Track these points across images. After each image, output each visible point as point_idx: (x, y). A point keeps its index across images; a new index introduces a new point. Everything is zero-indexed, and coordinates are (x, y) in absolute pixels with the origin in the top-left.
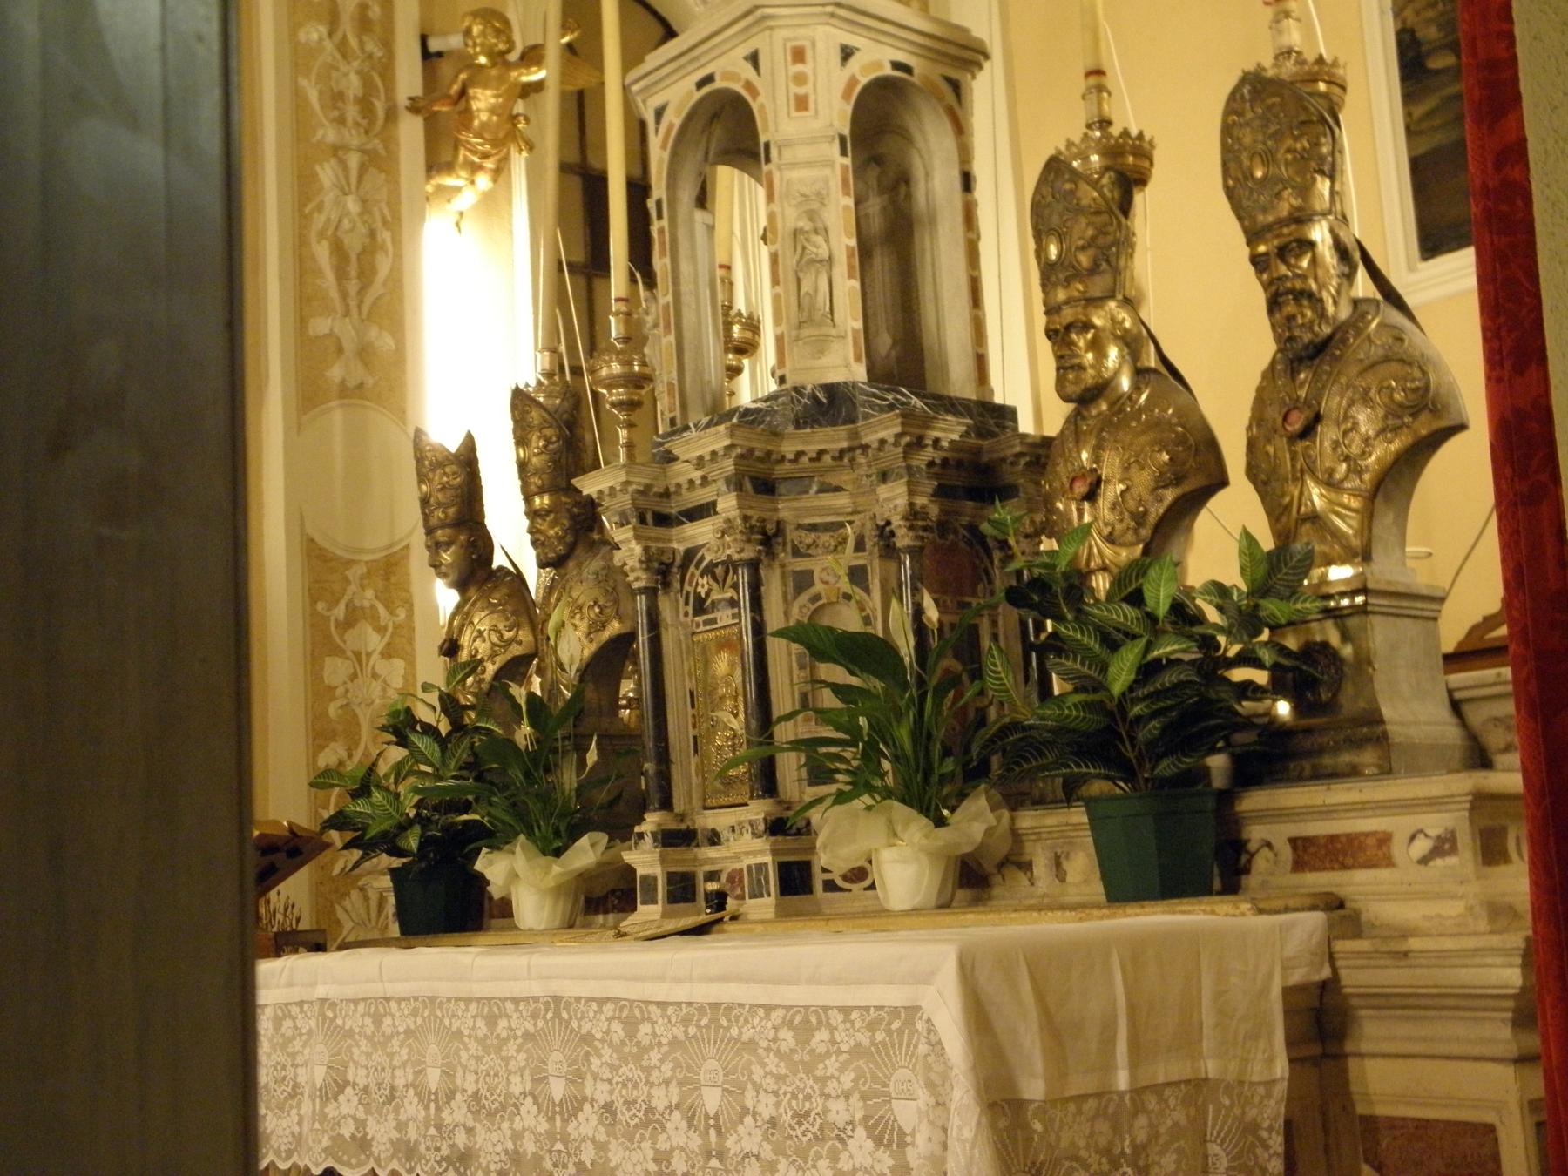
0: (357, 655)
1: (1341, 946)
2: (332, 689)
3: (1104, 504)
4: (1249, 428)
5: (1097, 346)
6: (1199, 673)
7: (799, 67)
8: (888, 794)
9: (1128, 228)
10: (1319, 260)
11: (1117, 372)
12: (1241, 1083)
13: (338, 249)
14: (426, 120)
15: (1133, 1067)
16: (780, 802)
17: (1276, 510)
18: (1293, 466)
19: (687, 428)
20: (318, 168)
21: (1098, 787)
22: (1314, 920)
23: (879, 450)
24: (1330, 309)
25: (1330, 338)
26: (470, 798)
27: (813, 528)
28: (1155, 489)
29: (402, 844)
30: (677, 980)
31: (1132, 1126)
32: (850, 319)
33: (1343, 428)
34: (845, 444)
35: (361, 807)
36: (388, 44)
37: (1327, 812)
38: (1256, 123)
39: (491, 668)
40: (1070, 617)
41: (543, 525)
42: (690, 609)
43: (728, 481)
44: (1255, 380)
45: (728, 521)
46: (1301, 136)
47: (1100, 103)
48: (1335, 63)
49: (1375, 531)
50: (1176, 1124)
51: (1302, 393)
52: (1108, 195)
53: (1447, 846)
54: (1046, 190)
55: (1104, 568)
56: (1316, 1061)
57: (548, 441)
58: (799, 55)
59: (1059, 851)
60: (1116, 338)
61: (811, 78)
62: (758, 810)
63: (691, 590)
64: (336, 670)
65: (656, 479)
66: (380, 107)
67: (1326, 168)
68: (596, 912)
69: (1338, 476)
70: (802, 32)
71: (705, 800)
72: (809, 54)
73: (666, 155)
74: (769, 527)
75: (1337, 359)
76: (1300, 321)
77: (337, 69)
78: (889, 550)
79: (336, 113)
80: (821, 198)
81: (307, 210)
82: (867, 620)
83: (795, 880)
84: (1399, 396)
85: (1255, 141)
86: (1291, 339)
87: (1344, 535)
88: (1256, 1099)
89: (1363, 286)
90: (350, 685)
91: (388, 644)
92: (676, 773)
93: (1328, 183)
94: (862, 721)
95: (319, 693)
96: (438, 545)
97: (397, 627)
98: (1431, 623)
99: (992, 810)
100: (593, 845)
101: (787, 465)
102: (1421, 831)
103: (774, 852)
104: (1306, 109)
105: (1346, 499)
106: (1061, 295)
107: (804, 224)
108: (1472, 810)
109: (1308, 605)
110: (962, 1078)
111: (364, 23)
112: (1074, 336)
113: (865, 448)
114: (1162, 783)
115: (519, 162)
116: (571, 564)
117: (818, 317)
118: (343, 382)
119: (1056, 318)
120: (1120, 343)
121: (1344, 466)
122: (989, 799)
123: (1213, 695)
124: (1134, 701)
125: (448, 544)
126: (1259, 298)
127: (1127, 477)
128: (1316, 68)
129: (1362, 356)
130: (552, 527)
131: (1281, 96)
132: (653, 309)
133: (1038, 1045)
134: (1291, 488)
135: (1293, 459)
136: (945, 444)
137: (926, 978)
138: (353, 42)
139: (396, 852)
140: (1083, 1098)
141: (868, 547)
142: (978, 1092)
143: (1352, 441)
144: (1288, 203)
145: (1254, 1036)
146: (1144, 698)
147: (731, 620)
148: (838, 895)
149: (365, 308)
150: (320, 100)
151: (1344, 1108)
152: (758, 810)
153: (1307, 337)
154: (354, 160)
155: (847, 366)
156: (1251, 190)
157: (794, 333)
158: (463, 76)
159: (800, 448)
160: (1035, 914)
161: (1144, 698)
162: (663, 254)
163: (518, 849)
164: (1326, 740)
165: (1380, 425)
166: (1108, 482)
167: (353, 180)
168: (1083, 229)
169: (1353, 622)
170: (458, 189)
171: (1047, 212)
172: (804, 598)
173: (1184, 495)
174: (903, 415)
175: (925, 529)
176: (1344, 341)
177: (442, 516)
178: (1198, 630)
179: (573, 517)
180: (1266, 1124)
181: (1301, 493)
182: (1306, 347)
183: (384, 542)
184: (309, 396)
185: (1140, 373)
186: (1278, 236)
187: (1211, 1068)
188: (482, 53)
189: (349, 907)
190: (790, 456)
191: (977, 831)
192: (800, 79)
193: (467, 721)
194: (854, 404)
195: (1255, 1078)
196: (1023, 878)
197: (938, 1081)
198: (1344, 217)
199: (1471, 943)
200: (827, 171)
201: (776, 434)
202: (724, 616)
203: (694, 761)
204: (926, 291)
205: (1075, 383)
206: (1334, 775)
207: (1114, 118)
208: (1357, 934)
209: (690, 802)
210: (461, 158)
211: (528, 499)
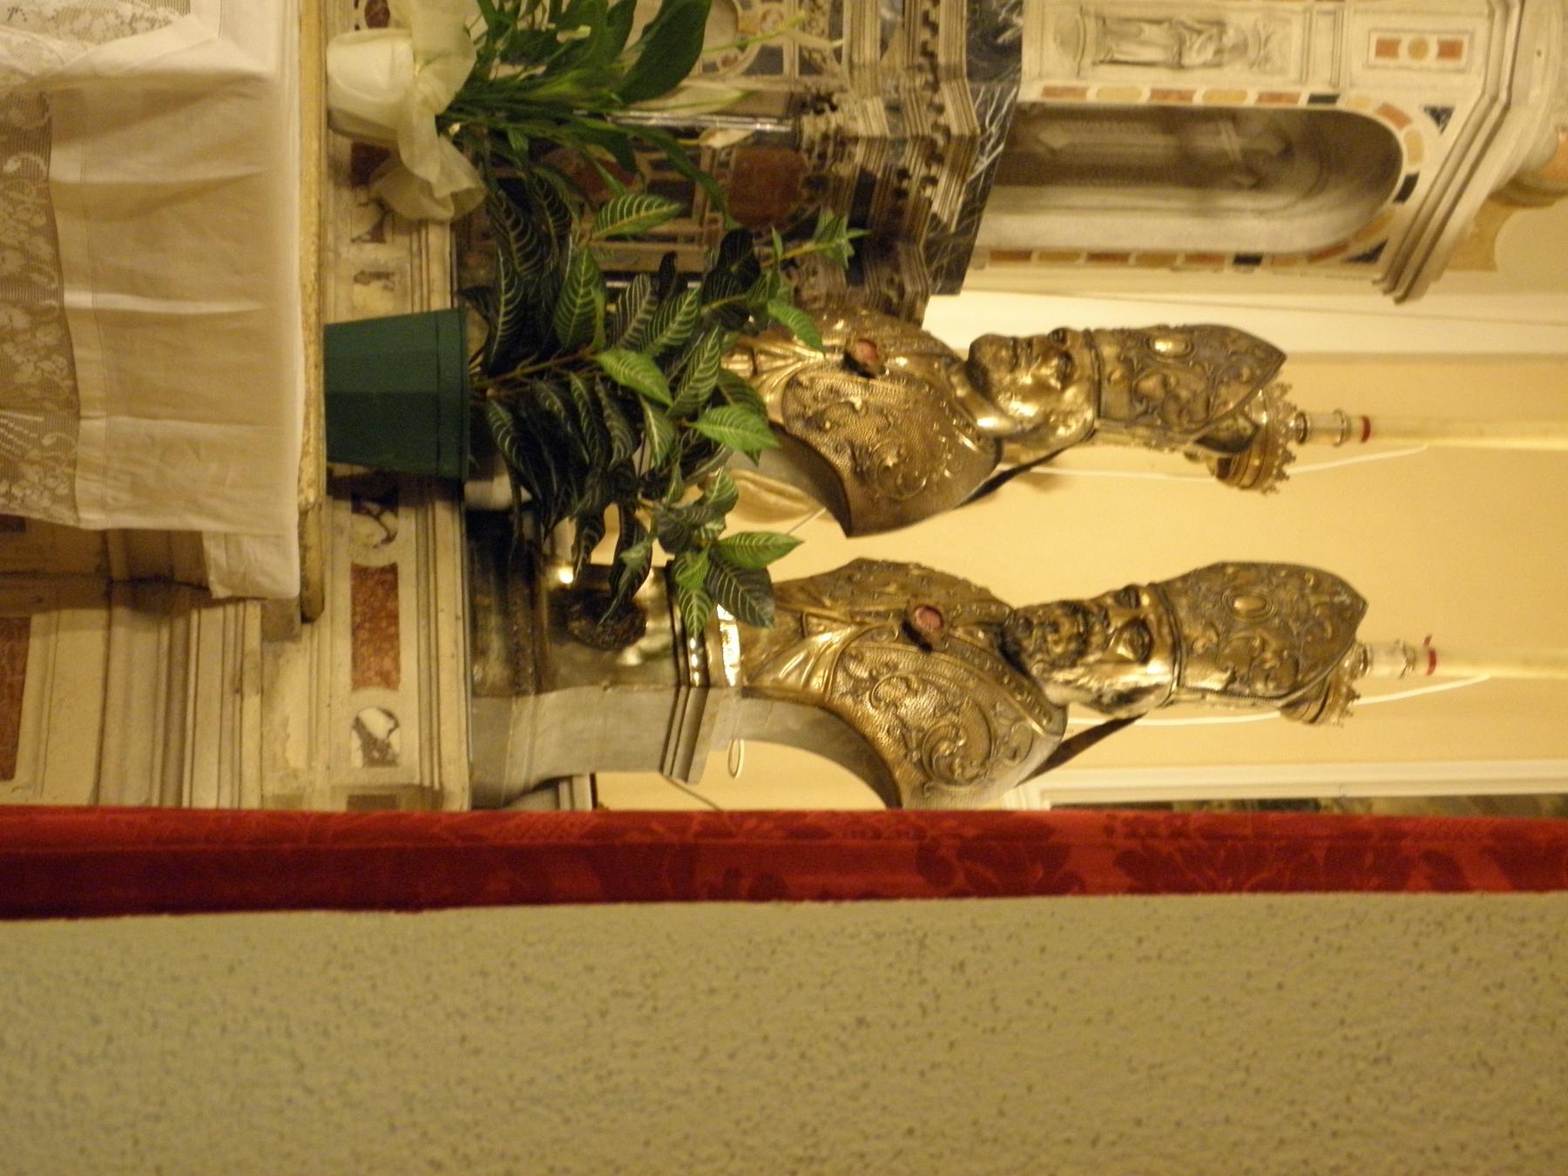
1: (253, 613)
3: (839, 379)
4: (918, 566)
5: (1040, 390)
6: (621, 465)
7: (1433, 49)
8: (484, 59)
10: (1127, 667)
11: (1003, 413)
12: (73, 464)
15: (99, 316)
17: (815, 588)
18: (870, 614)
21: (476, 337)
22: (290, 585)
23: (931, 105)
24: (1060, 676)
25: (1025, 672)
31: (14, 304)
32: (1104, 87)
33: (913, 678)
37: (428, 613)
38: (1303, 607)
40: (705, 310)
44: (978, 580)
46: (1281, 658)
47: (1329, 432)
48: (1345, 712)
49: (778, 705)
50: (16, 368)
52: (1224, 425)
53: (376, 754)
54: (1243, 345)
55: (756, 372)
56: (103, 571)
58: (1450, 50)
59: (396, 278)
60: (1047, 416)
61: (1416, 64)
67: (1236, 686)
69: (852, 666)
70: (1479, 58)
72: (1449, 64)
75: (999, 680)
76: (1050, 638)
78: (799, 105)
80: (1261, 63)
82: (710, 68)
84: (944, 748)
85: (1281, 604)
86: (1029, 625)
87: (778, 667)
88: (50, 482)
89: (1081, 720)
94: (584, 31)
98: (658, 763)
99: (455, 196)
102: (397, 725)
104: (1313, 667)
107: (1230, 38)
108: (421, 788)
110: (83, 54)
112: (1055, 362)
113: (935, 87)
114: (480, 416)
117: (1110, 42)
119: (1081, 341)
120: (1039, 420)
121: (865, 675)
122: (469, 192)
123: (589, 481)
124: (590, 383)
126: (1085, 589)
128: (1344, 690)
129: (999, 708)
133: (130, 179)
135: (878, 614)
136: (929, 192)
137: (230, 27)
140: (54, 239)
142: (60, 77)
144: (1199, 636)
145: (136, 487)
146: (592, 392)
151: (40, 600)
153: (1029, 645)
155: (1040, 76)
160: (314, 229)
161: (592, 392)
164: (520, 621)
165: (911, 722)
166: (866, 387)
168: (1189, 385)
169: (667, 668)
171: (1216, 344)
173: (840, 480)
174: (973, 139)
175: (822, 156)
176: (1020, 689)
178: (677, 471)
180: (16, 491)
181: (834, 620)
182: (1017, 642)
185: (996, 442)
186: (1159, 621)
187: (94, 425)
192: (1418, 49)
194: (991, 79)
195: (79, 484)
196: (362, 229)
197: (79, 25)
198: (1172, 703)
199: (250, 771)
200: (1293, 74)
204: (1114, 197)
208: (266, 636)
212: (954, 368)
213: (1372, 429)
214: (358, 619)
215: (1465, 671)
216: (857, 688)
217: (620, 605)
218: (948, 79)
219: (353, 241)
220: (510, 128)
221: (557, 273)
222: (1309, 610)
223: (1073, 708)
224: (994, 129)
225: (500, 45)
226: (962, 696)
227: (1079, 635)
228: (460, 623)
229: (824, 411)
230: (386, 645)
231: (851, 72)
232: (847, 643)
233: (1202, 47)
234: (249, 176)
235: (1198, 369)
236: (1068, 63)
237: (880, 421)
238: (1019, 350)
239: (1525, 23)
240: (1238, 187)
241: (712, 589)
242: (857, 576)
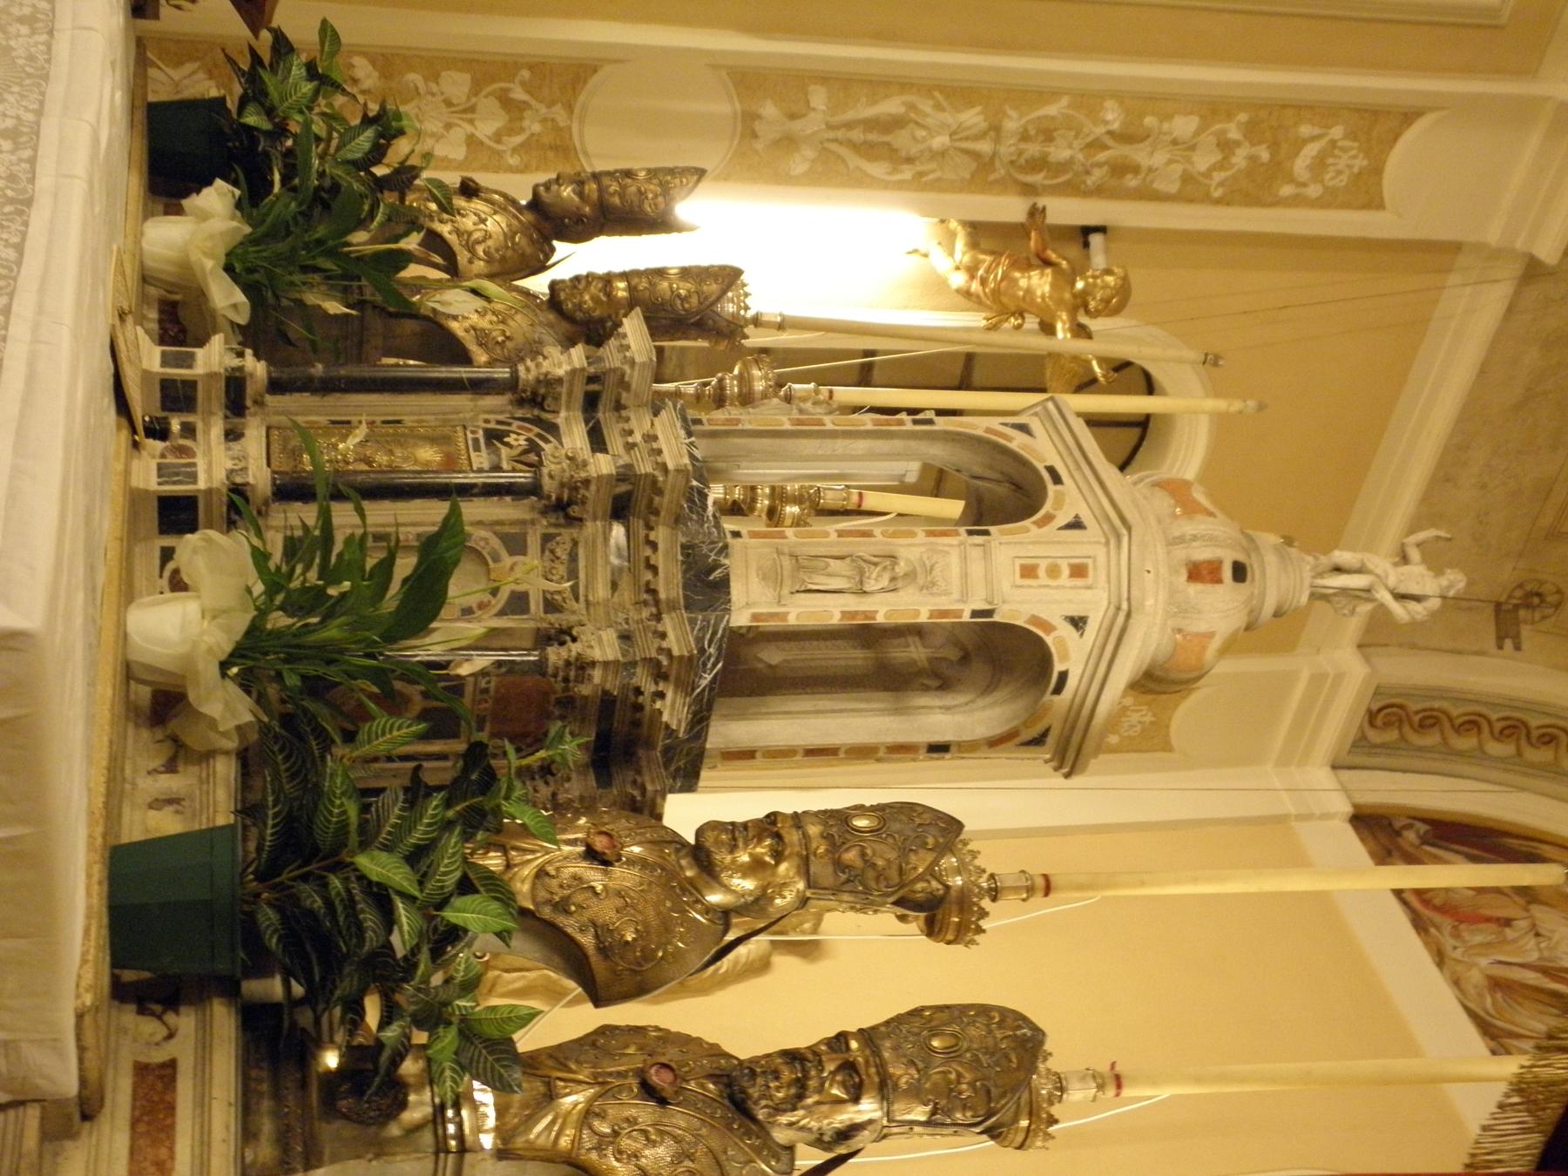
0: (472, 109)
1: (32, 1115)
2: (436, 78)
4: (657, 1029)
5: (756, 866)
7: (1066, 571)
8: (262, 614)
9: (883, 904)
10: (839, 1107)
11: (727, 889)
13: (896, 123)
14: (1022, 225)
16: (266, 503)
17: (561, 1056)
18: (610, 1074)
19: (690, 434)
20: (979, 109)
24: (784, 1119)
25: (753, 1119)
26: (297, 181)
27: (573, 558)
28: (595, 925)
29: (251, 108)
30: (36, 327)
32: (801, 612)
34: (662, 595)
35: (298, 71)
36: (1099, 192)
38: (990, 1041)
39: (445, 230)
40: (450, 814)
41: (595, 288)
42: (492, 425)
43: (629, 467)
44: (710, 1038)
45: (585, 464)
46: (975, 1090)
47: (1016, 889)
48: (1048, 1136)
49: (530, 1165)
51: (692, 1086)
54: (927, 817)
55: (508, 866)
57: (683, 299)
58: (1078, 571)
60: (764, 889)
61: (1053, 583)
62: (259, 476)
63: (513, 428)
64: (456, 85)
65: (637, 395)
66: (1037, 178)
68: (161, 312)
69: (596, 1123)
70: (1103, 577)
71: (278, 428)
72: (1079, 582)
73: (979, 432)
74: (576, 508)
75: (729, 1127)
77: (1076, 137)
78: (545, 638)
79: (1032, 132)
80: (929, 587)
81: (936, 94)
83: (177, 514)
86: (753, 1074)
90: (441, 98)
91: (482, 143)
92: (305, 399)
93: (923, 1118)
95: (434, 64)
96: (581, 183)
97: (500, 154)
99: (239, 728)
100: (235, 306)
101: (642, 532)
103: (209, 492)
104: (1003, 1095)
105: (570, 1132)
106: (814, 830)
107: (901, 568)
109: (449, 1083)
111: (1121, 169)
112: (768, 842)
113: (658, 617)
115: (976, 319)
116: (551, 317)
117: (801, 575)
118: (759, 117)
119: (790, 822)
120: (758, 893)
123: (347, 970)
124: (346, 880)
125: (581, 194)
127: (610, 895)
130: (592, 298)
131: (1018, 1069)
132: (818, 410)
134: (587, 1072)
135: (619, 1074)
136: (658, 705)
138: (1102, 156)
139: (243, 103)
141: (549, 616)
143: (635, 1140)
144: (902, 1074)
146: (348, 891)
147: (478, 465)
148: (157, 562)
149: (833, 147)
150: (1046, 117)
152: (259, 476)
153: (754, 1092)
154: (985, 147)
156: (918, 1034)
157: (786, 550)
158: (1064, 264)
159: (661, 546)
161: (348, 891)
162: (876, 423)
163: (235, 224)
166: (606, 873)
167: (965, 145)
168: (883, 855)
170: (951, 254)
172: (496, 543)
173: (586, 956)
174: (691, 658)
176: (748, 1133)
177: (612, 189)
178: (424, 957)
179: (602, 321)
181: (580, 1082)
182: (743, 1091)
183: (590, 149)
184: (747, 80)
185: (725, 915)
186: (867, 1062)
188: (1087, 284)
189: (196, 77)
190: (652, 537)
191: (213, 707)
192: (1053, 572)
193: (386, 193)
196: (157, 763)
198: (885, 1137)
200: (956, 596)
201: (678, 520)
202: (481, 459)
203: (323, 420)
204: (824, 702)
205: (718, 842)
206: (247, 1109)
207: (1000, 903)
209: (277, 413)
210: (982, 257)
211: (625, 276)
212: (683, 852)
213: (1053, 884)
214: (137, 1113)
215: (1148, 1092)
216: (601, 1144)
217: (383, 1083)
218: (669, 612)
219: (149, 773)
220: (285, 668)
221: (317, 787)
222: (996, 1044)
223: (801, 1149)
224: (712, 650)
225: (279, 598)
226: (696, 1144)
227: (798, 1080)
228: (233, 1109)
229: (569, 897)
230: (162, 1136)
231: (587, 609)
232: (590, 1101)
233: (879, 575)
234: (19, 718)
235: (890, 840)
236: (770, 594)
237: (619, 902)
238: (736, 833)
239: (1134, 548)
240: (926, 689)
241: (463, 1061)
242: (599, 1042)
